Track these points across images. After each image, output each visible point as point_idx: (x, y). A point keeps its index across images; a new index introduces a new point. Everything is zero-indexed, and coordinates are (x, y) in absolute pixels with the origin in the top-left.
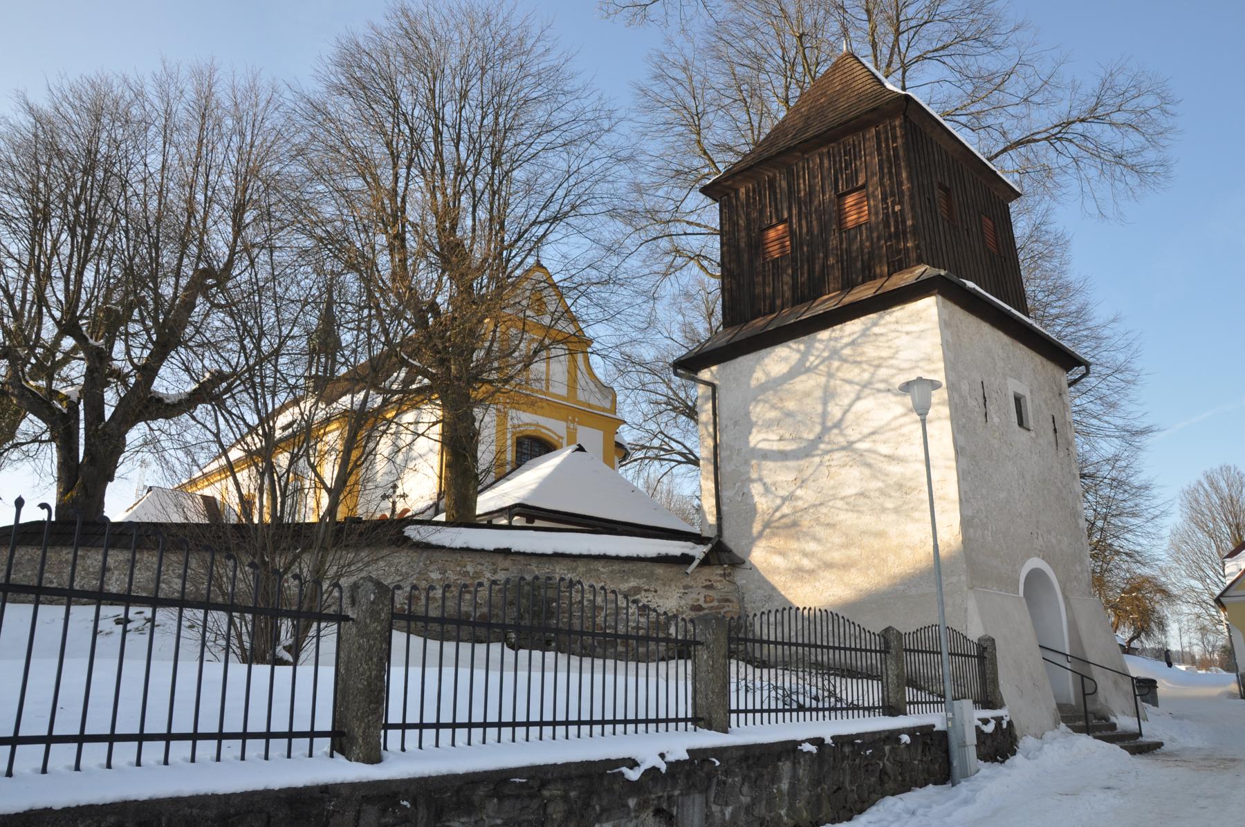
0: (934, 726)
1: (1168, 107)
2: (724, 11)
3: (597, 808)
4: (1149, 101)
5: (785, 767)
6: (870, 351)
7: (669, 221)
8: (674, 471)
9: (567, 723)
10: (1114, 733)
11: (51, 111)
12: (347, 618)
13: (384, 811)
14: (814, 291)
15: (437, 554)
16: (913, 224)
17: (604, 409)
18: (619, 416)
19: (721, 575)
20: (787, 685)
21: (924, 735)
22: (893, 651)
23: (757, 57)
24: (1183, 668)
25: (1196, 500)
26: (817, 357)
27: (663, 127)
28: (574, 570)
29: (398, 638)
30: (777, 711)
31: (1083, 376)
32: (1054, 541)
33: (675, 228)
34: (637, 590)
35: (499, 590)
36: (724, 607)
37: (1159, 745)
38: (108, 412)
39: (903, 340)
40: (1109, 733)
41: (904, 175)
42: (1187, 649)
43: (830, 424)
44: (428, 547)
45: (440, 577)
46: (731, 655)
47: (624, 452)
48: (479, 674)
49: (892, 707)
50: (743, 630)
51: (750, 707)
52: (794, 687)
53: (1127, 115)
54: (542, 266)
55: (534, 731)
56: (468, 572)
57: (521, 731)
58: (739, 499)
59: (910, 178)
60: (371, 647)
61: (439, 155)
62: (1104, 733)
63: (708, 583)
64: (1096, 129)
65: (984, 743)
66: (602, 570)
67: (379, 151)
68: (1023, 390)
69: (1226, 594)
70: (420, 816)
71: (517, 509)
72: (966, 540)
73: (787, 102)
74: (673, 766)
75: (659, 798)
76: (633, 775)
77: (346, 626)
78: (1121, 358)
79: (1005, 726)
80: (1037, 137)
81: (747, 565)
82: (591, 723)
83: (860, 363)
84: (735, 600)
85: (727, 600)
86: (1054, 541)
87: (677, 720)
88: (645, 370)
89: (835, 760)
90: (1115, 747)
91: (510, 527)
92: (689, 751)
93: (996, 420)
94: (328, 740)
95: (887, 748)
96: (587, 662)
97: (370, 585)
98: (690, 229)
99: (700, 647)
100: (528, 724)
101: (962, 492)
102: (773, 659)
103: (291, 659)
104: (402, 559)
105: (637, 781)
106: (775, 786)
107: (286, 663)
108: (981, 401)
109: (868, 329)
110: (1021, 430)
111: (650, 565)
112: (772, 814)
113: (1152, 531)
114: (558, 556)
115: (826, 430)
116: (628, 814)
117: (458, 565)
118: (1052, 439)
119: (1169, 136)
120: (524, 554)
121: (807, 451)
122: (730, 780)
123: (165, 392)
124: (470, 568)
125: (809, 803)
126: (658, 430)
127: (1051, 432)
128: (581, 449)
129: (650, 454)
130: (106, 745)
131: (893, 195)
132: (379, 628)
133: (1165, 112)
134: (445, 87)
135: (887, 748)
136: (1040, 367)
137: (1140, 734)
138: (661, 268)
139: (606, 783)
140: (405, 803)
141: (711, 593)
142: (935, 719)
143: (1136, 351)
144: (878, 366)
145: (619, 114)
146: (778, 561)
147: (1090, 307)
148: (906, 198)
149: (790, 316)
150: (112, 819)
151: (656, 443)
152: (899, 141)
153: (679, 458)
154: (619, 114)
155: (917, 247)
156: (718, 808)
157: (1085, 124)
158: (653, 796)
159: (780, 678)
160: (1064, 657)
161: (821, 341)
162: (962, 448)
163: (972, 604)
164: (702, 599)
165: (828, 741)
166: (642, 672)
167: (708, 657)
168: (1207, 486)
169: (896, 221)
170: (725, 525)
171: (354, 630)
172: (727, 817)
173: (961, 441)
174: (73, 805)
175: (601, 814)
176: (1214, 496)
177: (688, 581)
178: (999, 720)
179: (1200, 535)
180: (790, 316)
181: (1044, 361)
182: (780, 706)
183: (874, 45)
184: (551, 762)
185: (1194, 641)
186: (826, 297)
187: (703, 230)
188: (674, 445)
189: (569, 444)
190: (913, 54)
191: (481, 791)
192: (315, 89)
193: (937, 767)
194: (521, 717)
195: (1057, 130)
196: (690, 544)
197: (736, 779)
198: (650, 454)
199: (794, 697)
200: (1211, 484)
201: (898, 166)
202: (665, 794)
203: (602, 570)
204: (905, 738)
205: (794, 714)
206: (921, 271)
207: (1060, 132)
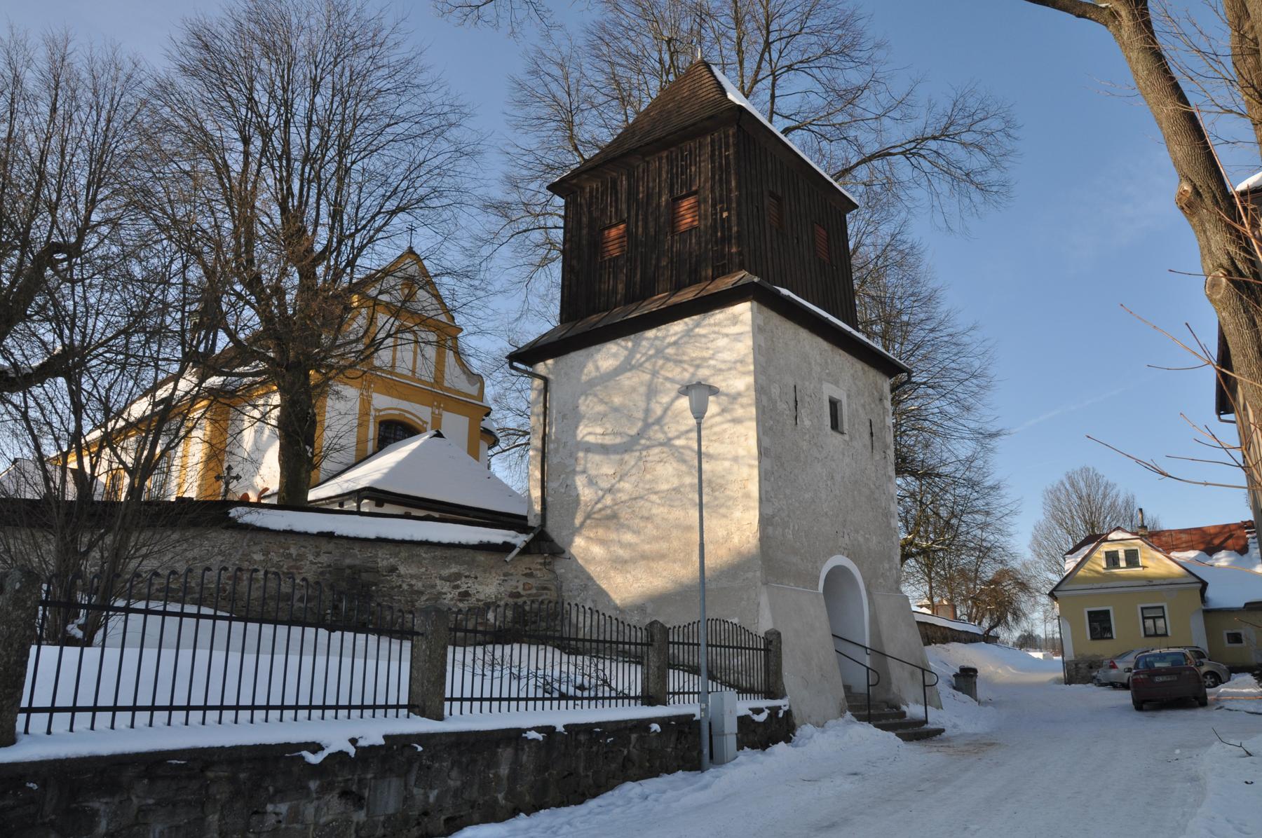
0: (694, 715)
1: (1011, 132)
2: (598, 13)
3: (271, 789)
4: (994, 124)
5: (506, 754)
6: (693, 352)
7: (538, 215)
10: (902, 721)
14: (647, 291)
15: (262, 536)
16: (738, 232)
19: (541, 564)
21: (684, 727)
22: (656, 644)
25: (1058, 500)
26: (643, 355)
27: (536, 122)
28: (396, 555)
30: (535, 699)
32: (861, 539)
34: (458, 576)
35: (229, 578)
36: (542, 595)
39: (722, 342)
40: (897, 721)
41: (733, 184)
43: (651, 420)
45: (262, 558)
48: (219, 656)
49: (651, 697)
50: (559, 618)
53: (974, 135)
54: (414, 253)
56: (291, 555)
58: (563, 491)
59: (739, 187)
62: (884, 722)
63: (528, 571)
64: (948, 148)
65: (754, 731)
66: (424, 555)
68: (840, 394)
69: (1059, 588)
71: (365, 493)
72: (764, 538)
79: (781, 715)
80: (893, 151)
83: (681, 362)
84: (553, 588)
85: (545, 588)
89: (566, 747)
90: (892, 735)
93: (807, 423)
99: (420, 638)
100: (518, 699)
101: (763, 492)
104: (225, 539)
106: (493, 771)
108: (792, 404)
109: (692, 330)
110: (834, 433)
112: (487, 798)
114: (381, 541)
115: (647, 426)
117: (282, 547)
118: (868, 442)
120: (347, 538)
121: (625, 448)
124: (293, 551)
127: (867, 436)
128: (439, 435)
130: (130, 713)
131: (721, 202)
132: (23, 616)
134: (301, 72)
135: (634, 736)
136: (860, 373)
137: (926, 722)
138: (537, 260)
139: (282, 765)
140: (31, 785)
141: (531, 581)
144: (698, 367)
146: (597, 550)
148: (734, 205)
152: (731, 151)
155: (740, 253)
156: (422, 791)
157: (939, 142)
158: (340, 779)
161: (647, 339)
162: (766, 449)
163: (764, 600)
165: (560, 728)
167: (427, 647)
168: (1068, 486)
169: (723, 227)
170: (549, 515)
172: (432, 799)
173: (767, 442)
176: (1074, 496)
177: (508, 568)
179: (1059, 532)
180: (619, 315)
181: (866, 367)
182: (540, 695)
183: (740, 52)
186: (656, 297)
195: (913, 145)
196: (513, 533)
197: (445, 764)
199: (556, 685)
200: (1073, 485)
201: (728, 173)
202: (356, 777)
203: (424, 555)
204: (655, 727)
205: (555, 703)
207: (915, 148)
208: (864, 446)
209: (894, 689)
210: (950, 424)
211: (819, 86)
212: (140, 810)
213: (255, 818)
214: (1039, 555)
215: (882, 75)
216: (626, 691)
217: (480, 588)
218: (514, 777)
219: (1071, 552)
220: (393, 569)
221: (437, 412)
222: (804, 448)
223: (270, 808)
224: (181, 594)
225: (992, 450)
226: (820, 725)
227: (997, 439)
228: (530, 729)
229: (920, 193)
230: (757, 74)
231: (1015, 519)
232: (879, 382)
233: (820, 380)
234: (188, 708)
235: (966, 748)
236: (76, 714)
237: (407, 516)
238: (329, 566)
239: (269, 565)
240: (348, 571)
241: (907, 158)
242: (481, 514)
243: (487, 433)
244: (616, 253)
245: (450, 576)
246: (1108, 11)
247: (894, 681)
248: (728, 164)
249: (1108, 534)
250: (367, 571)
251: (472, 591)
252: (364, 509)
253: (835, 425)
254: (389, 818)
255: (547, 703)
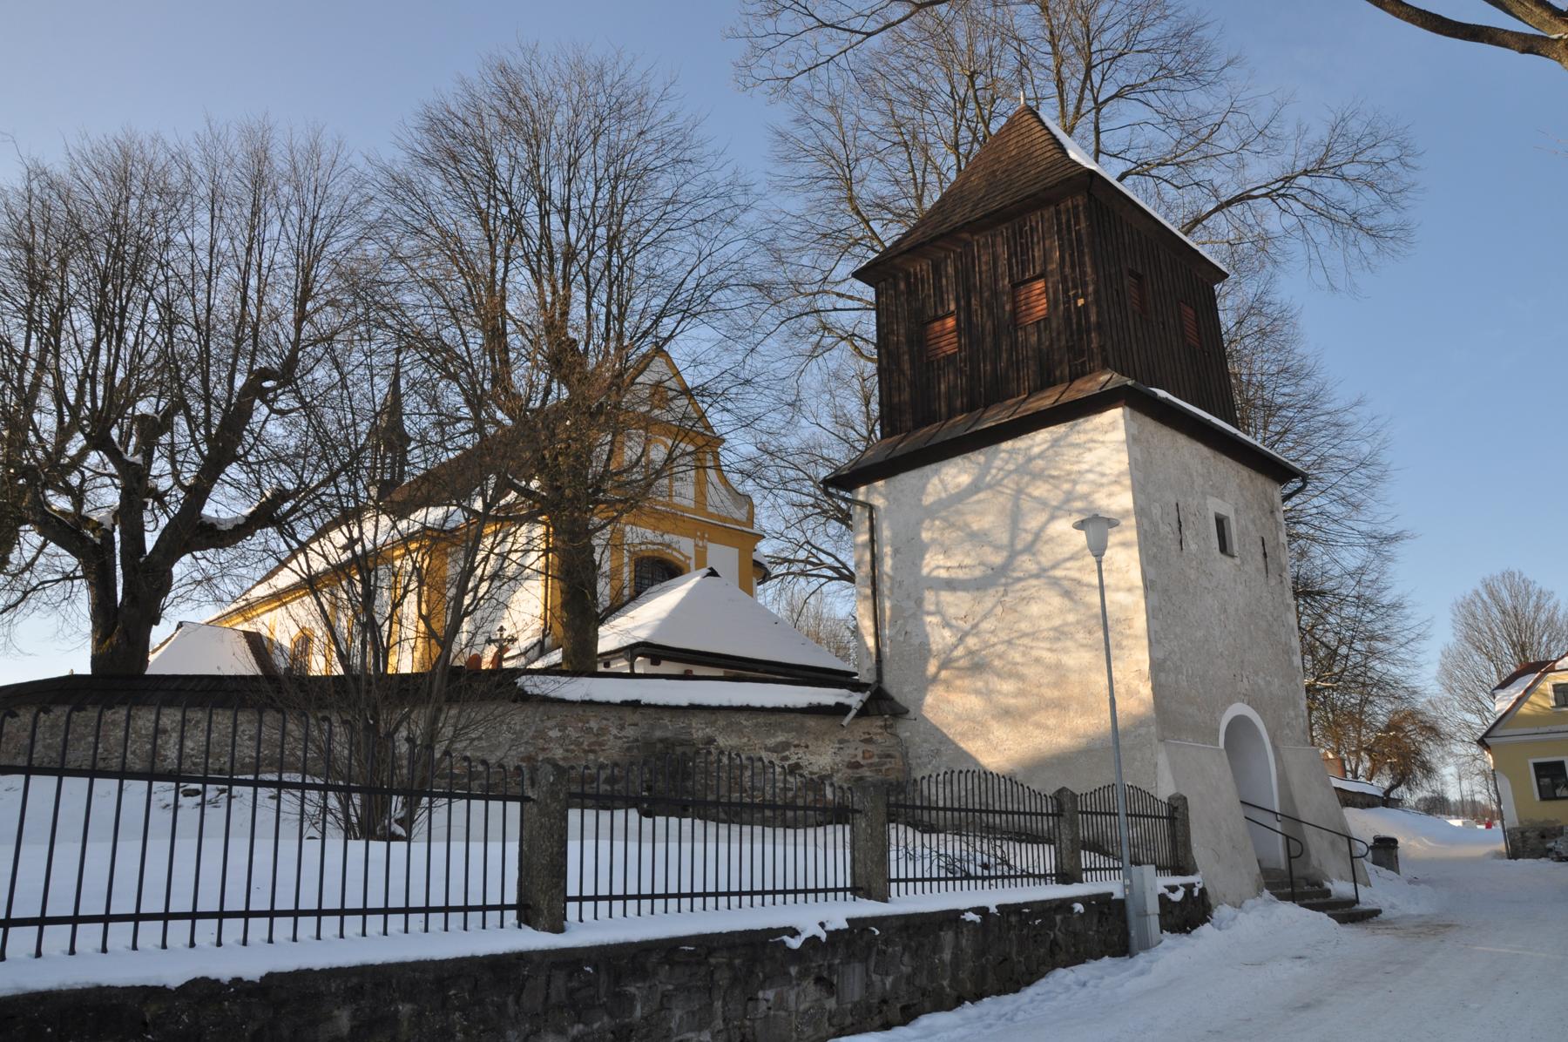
0: (1112, 894)
1: (1408, 160)
3: (761, 975)
4: (1386, 152)
5: (948, 937)
8: (824, 588)
9: (717, 894)
11: (68, 178)
12: (528, 799)
13: (570, 976)
15: (557, 708)
17: (737, 522)
18: (756, 530)
19: (881, 727)
20: (950, 852)
21: (1103, 906)
22: (1066, 814)
23: (921, 92)
24: (1457, 823)
25: (1474, 616)
28: (713, 724)
29: (574, 815)
31: (1299, 490)
32: (1262, 683)
33: (822, 302)
34: (786, 746)
36: (885, 763)
37: (1376, 912)
38: (150, 541)
40: (1321, 900)
42: (1469, 798)
44: (545, 700)
45: (559, 734)
46: (892, 818)
47: (763, 572)
48: (458, 847)
51: (911, 876)
52: (957, 852)
55: (698, 901)
56: (591, 729)
57: (659, 903)
58: (902, 639)
60: (552, 826)
61: (545, 236)
62: (1307, 901)
64: (1326, 185)
65: (1171, 912)
66: (745, 723)
67: (472, 233)
68: (1226, 510)
69: (1492, 734)
70: (601, 980)
73: (957, 149)
74: (832, 935)
75: (820, 966)
76: (795, 943)
77: (528, 805)
78: (1366, 449)
79: (1196, 893)
80: (1255, 193)
81: (912, 715)
82: (740, 894)
84: (897, 754)
85: (889, 756)
86: (1262, 683)
87: (836, 890)
88: (787, 465)
90: (1323, 915)
91: (632, 675)
92: (848, 920)
93: (1193, 547)
94: (514, 913)
95: (1058, 918)
96: (735, 828)
97: (549, 768)
98: (840, 303)
99: (858, 815)
101: (1152, 633)
102: (941, 822)
103: (404, 834)
104: (518, 718)
105: (798, 950)
107: (398, 838)
108: (1176, 525)
111: (799, 717)
113: (1407, 657)
114: (694, 708)
116: (790, 982)
117: (580, 721)
118: (1262, 565)
119: (1410, 195)
120: (656, 706)
122: (890, 950)
123: (214, 515)
124: (593, 724)
125: (973, 974)
126: (803, 540)
127: (1260, 557)
128: (713, 573)
129: (794, 568)
131: (1075, 287)
133: (1405, 165)
135: (1058, 918)
136: (1247, 482)
137: (1357, 901)
141: (870, 748)
142: (1113, 886)
143: (1385, 441)
145: (756, 189)
147: (1328, 387)
149: (960, 424)
150: (355, 980)
151: (802, 555)
152: (1083, 225)
153: (830, 573)
154: (756, 189)
156: (879, 977)
159: (950, 845)
160: (1273, 816)
162: (1152, 582)
163: (1162, 759)
164: (860, 755)
165: (993, 910)
166: (790, 839)
168: (1485, 597)
170: (886, 669)
171: (535, 810)
172: (888, 986)
173: (1152, 574)
174: (327, 967)
175: (764, 981)
176: (1495, 610)
177: (844, 734)
178: (1189, 888)
179: (1476, 658)
180: (960, 424)
181: (1253, 474)
182: (942, 875)
184: (717, 930)
185: (1477, 788)
187: (856, 304)
188: (823, 557)
189: (698, 567)
190: (1109, 90)
191: (654, 959)
192: (400, 161)
193: (1115, 938)
194: (673, 889)
196: (845, 691)
198: (794, 568)
200: (1491, 594)
201: (1081, 254)
203: (745, 723)
204: (1079, 907)
205: (958, 883)
206: (1106, 379)
207: (1283, 187)
208: (1258, 569)
209: (1314, 862)
210: (1335, 526)
211: (1156, 115)
212: (664, 995)
213: (750, 1004)
214: (1451, 690)
215: (1241, 104)
216: (1031, 871)
217: (813, 759)
218: (956, 962)
219: (1504, 685)
220: (711, 741)
221: (701, 544)
222: (1192, 577)
223: (760, 994)
224: (466, 780)
225: (1389, 559)
226: (1238, 905)
227: (1397, 544)
228: (967, 911)
229: (1296, 247)
230: (1078, 108)
231: (1424, 645)
232: (1269, 490)
233: (1204, 494)
234: (386, 911)
235: (1418, 930)
236: (389, 916)
237: (687, 676)
238: (636, 740)
239: (567, 742)
240: (659, 746)
241: (1273, 200)
242: (783, 670)
243: (758, 565)
244: (950, 350)
245: (778, 745)
246: (1562, 43)
247: (1313, 851)
248: (1079, 240)
249: (1556, 661)
250: (681, 745)
251: (803, 763)
252: (638, 670)
253: (1224, 548)
254: (855, 1005)
255: (950, 883)
